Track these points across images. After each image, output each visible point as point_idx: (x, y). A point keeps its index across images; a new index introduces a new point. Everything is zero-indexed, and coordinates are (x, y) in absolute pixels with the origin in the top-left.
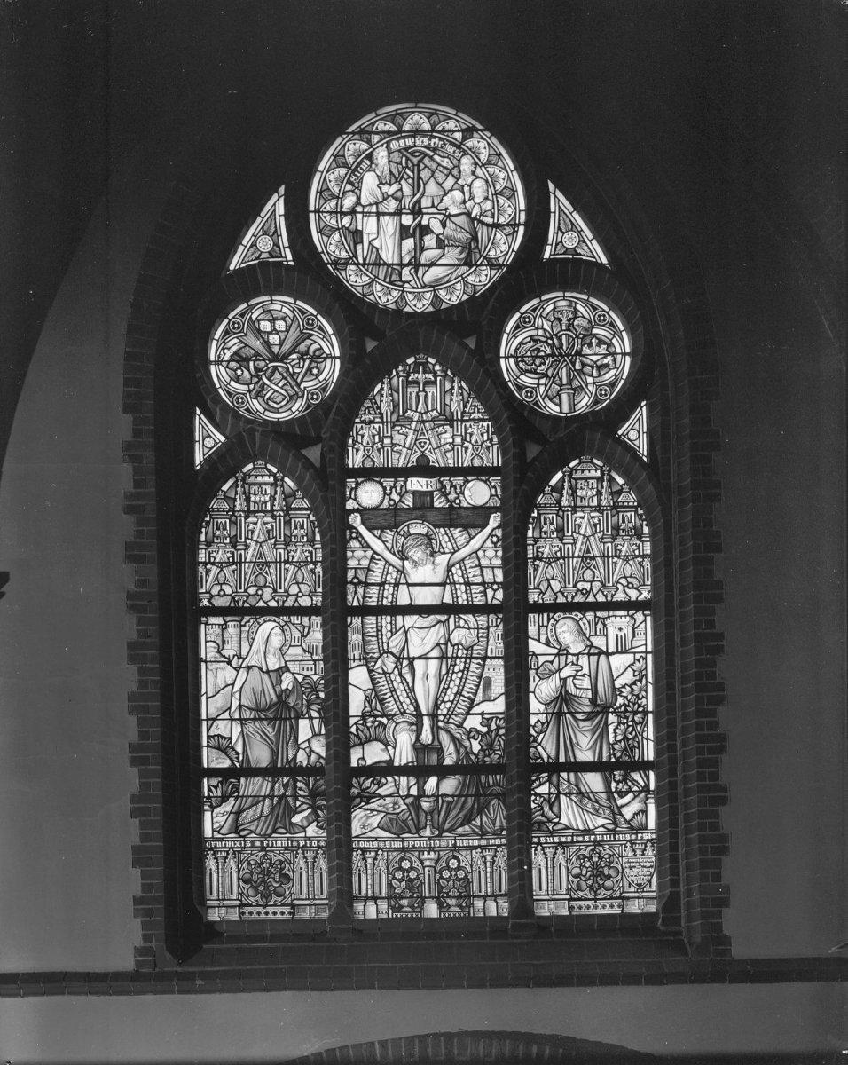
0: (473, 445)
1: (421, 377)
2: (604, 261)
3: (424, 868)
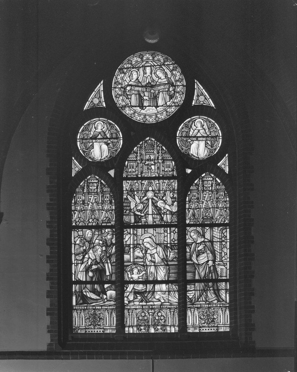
2: (213, 106)
3: (149, 316)
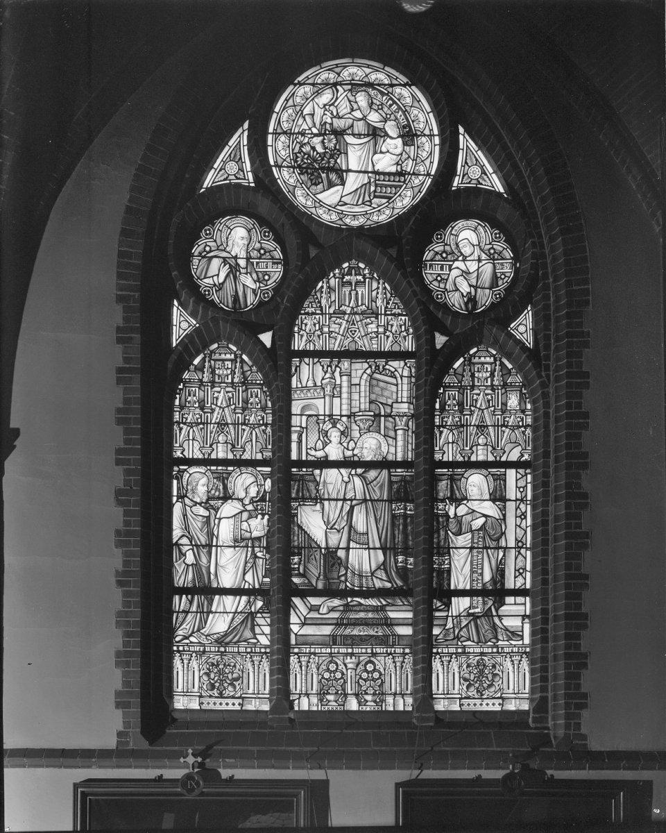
0: (307, 334)
1: (353, 278)
2: (502, 190)
3: (347, 670)
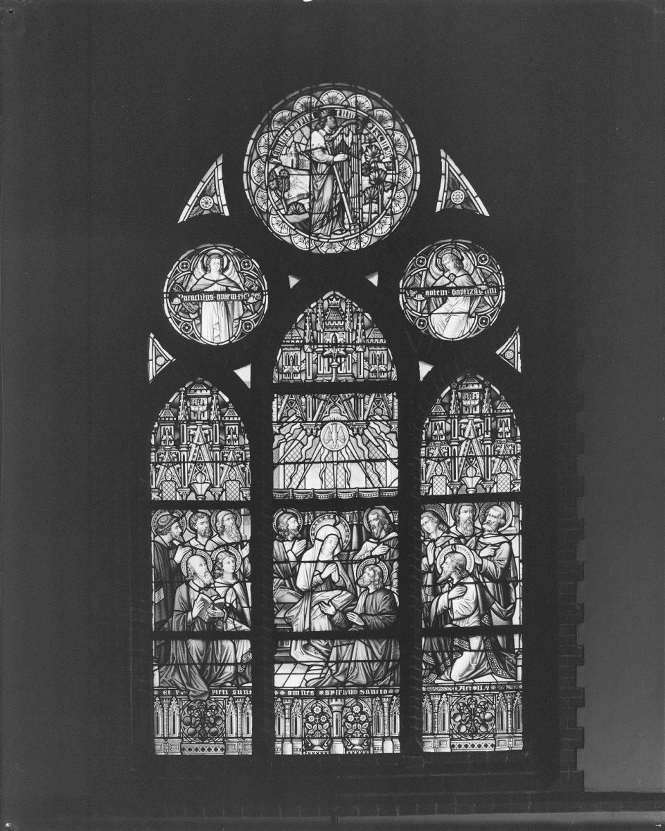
3: (332, 713)
